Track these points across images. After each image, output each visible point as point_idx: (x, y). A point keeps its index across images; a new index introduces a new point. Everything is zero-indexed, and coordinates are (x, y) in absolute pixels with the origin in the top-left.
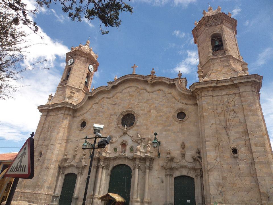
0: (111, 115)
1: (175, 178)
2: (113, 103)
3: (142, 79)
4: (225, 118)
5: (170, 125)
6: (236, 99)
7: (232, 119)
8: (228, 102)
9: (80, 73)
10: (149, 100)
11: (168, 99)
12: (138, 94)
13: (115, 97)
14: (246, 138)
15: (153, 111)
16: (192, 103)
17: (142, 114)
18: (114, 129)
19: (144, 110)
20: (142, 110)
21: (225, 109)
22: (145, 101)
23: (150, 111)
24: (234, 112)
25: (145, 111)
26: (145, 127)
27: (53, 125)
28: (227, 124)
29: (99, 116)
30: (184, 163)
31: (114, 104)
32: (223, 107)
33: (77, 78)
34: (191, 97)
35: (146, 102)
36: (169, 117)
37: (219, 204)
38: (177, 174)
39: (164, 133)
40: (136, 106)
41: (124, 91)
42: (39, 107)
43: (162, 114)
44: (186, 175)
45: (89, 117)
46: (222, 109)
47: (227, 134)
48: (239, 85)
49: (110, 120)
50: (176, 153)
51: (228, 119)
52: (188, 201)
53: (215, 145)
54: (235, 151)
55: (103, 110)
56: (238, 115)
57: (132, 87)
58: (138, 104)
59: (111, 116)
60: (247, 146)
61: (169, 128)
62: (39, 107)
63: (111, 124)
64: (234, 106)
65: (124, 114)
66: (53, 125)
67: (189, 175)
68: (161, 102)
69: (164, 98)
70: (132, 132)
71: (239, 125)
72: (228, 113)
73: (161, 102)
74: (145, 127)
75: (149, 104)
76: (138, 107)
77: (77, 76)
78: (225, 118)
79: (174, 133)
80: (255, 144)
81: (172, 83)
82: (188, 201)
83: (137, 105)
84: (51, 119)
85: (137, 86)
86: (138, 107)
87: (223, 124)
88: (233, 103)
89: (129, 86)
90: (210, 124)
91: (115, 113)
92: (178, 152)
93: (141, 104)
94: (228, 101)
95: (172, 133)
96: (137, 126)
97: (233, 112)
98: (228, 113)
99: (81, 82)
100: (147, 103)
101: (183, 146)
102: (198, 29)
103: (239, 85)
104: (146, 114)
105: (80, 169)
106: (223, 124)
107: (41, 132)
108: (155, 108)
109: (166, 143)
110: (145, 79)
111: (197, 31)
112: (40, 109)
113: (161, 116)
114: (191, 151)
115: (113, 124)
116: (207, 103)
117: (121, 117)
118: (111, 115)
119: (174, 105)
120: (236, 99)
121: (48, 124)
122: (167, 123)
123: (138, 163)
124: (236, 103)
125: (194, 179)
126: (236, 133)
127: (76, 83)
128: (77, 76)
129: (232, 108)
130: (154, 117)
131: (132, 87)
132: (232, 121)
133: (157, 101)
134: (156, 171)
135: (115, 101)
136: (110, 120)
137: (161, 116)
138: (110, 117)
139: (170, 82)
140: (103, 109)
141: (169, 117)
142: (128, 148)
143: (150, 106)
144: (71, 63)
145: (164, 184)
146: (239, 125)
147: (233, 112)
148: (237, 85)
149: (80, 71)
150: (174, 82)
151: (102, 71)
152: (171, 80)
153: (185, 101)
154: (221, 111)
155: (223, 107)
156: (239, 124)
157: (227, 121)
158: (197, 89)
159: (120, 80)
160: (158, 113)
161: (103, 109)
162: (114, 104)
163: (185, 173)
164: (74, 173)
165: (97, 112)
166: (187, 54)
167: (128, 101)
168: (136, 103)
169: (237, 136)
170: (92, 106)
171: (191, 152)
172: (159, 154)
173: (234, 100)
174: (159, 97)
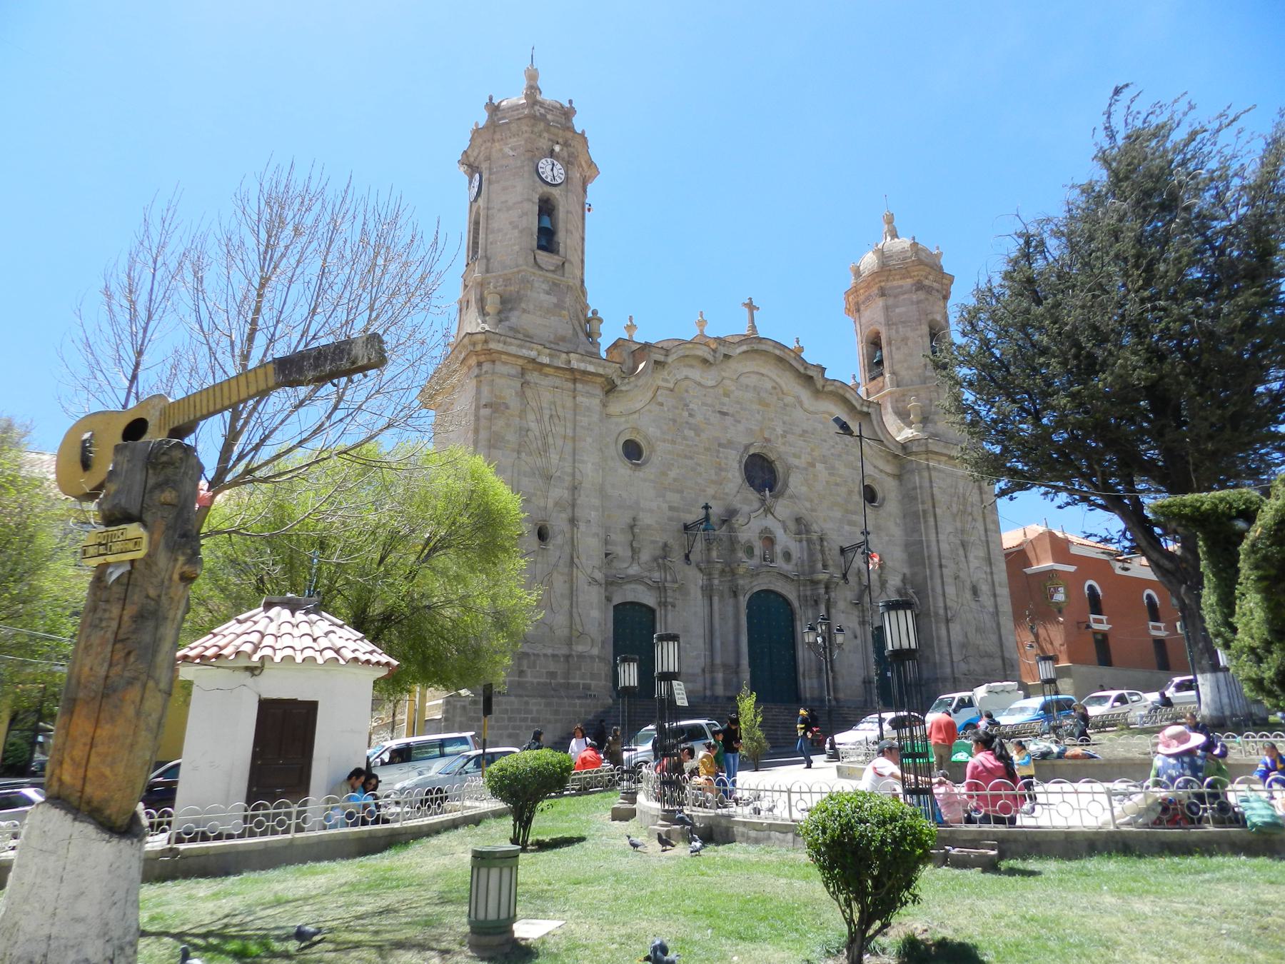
2: (718, 408)
3: (802, 370)
15: (819, 466)
16: (890, 472)
20: (795, 456)
29: (685, 438)
30: (634, 570)
34: (890, 458)
35: (801, 436)
37: (268, 960)
38: (617, 600)
39: (847, 528)
43: (838, 480)
58: (784, 436)
68: (833, 447)
73: (833, 447)
74: (808, 505)
81: (865, 409)
85: (778, 380)
86: (784, 444)
89: (756, 369)
93: (790, 438)
104: (806, 469)
105: (596, 571)
108: (824, 460)
110: (810, 373)
123: (163, 495)
131: (763, 375)
135: (724, 404)
142: (778, 549)
143: (812, 450)
145: (859, 641)
151: (1061, 619)
161: (691, 415)
168: (779, 431)
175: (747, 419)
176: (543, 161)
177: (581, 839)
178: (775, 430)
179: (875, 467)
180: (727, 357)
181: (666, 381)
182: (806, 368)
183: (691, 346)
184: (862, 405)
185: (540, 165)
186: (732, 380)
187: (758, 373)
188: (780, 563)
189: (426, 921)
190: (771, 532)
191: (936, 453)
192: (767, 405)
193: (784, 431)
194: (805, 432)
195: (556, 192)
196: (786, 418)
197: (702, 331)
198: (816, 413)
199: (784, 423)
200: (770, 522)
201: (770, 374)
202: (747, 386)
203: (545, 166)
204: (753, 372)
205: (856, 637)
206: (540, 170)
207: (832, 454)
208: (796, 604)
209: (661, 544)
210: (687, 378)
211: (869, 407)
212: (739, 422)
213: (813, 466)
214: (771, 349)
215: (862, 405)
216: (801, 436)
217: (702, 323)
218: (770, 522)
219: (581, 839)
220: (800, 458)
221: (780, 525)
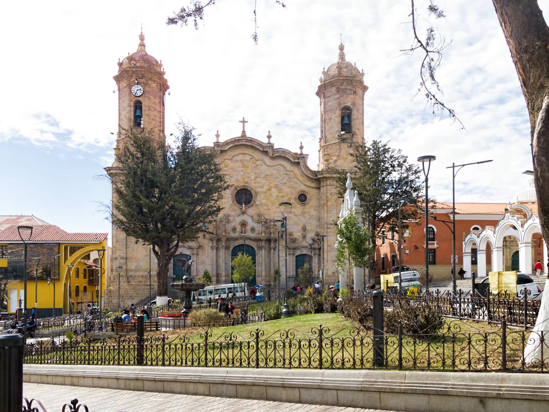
1: (297, 257)
3: (261, 149)
11: (290, 178)
12: (255, 165)
15: (273, 190)
17: (262, 192)
20: (260, 187)
22: (263, 176)
26: (266, 207)
35: (264, 178)
36: (291, 198)
38: (298, 253)
41: (235, 158)
50: (297, 235)
57: (245, 154)
69: (285, 176)
74: (266, 207)
77: (153, 119)
81: (297, 161)
85: (253, 154)
86: (255, 183)
89: (241, 152)
92: (300, 234)
93: (258, 180)
96: (257, 205)
101: (304, 229)
104: (266, 192)
119: (296, 185)
130: (275, 197)
131: (245, 154)
139: (294, 159)
141: (291, 198)
142: (248, 228)
143: (270, 183)
144: (136, 95)
150: (299, 161)
153: (309, 183)
163: (305, 252)
168: (253, 177)
175: (236, 175)
176: (134, 87)
178: (250, 177)
180: (222, 152)
182: (263, 148)
185: (133, 89)
188: (250, 234)
190: (245, 221)
192: (248, 167)
193: (255, 177)
194: (266, 175)
195: (140, 99)
196: (256, 171)
199: (256, 173)
200: (245, 217)
202: (237, 160)
203: (135, 89)
207: (281, 183)
208: (256, 249)
211: (298, 159)
212: (232, 177)
213: (270, 190)
216: (264, 178)
218: (245, 217)
220: (263, 187)
221: (250, 218)
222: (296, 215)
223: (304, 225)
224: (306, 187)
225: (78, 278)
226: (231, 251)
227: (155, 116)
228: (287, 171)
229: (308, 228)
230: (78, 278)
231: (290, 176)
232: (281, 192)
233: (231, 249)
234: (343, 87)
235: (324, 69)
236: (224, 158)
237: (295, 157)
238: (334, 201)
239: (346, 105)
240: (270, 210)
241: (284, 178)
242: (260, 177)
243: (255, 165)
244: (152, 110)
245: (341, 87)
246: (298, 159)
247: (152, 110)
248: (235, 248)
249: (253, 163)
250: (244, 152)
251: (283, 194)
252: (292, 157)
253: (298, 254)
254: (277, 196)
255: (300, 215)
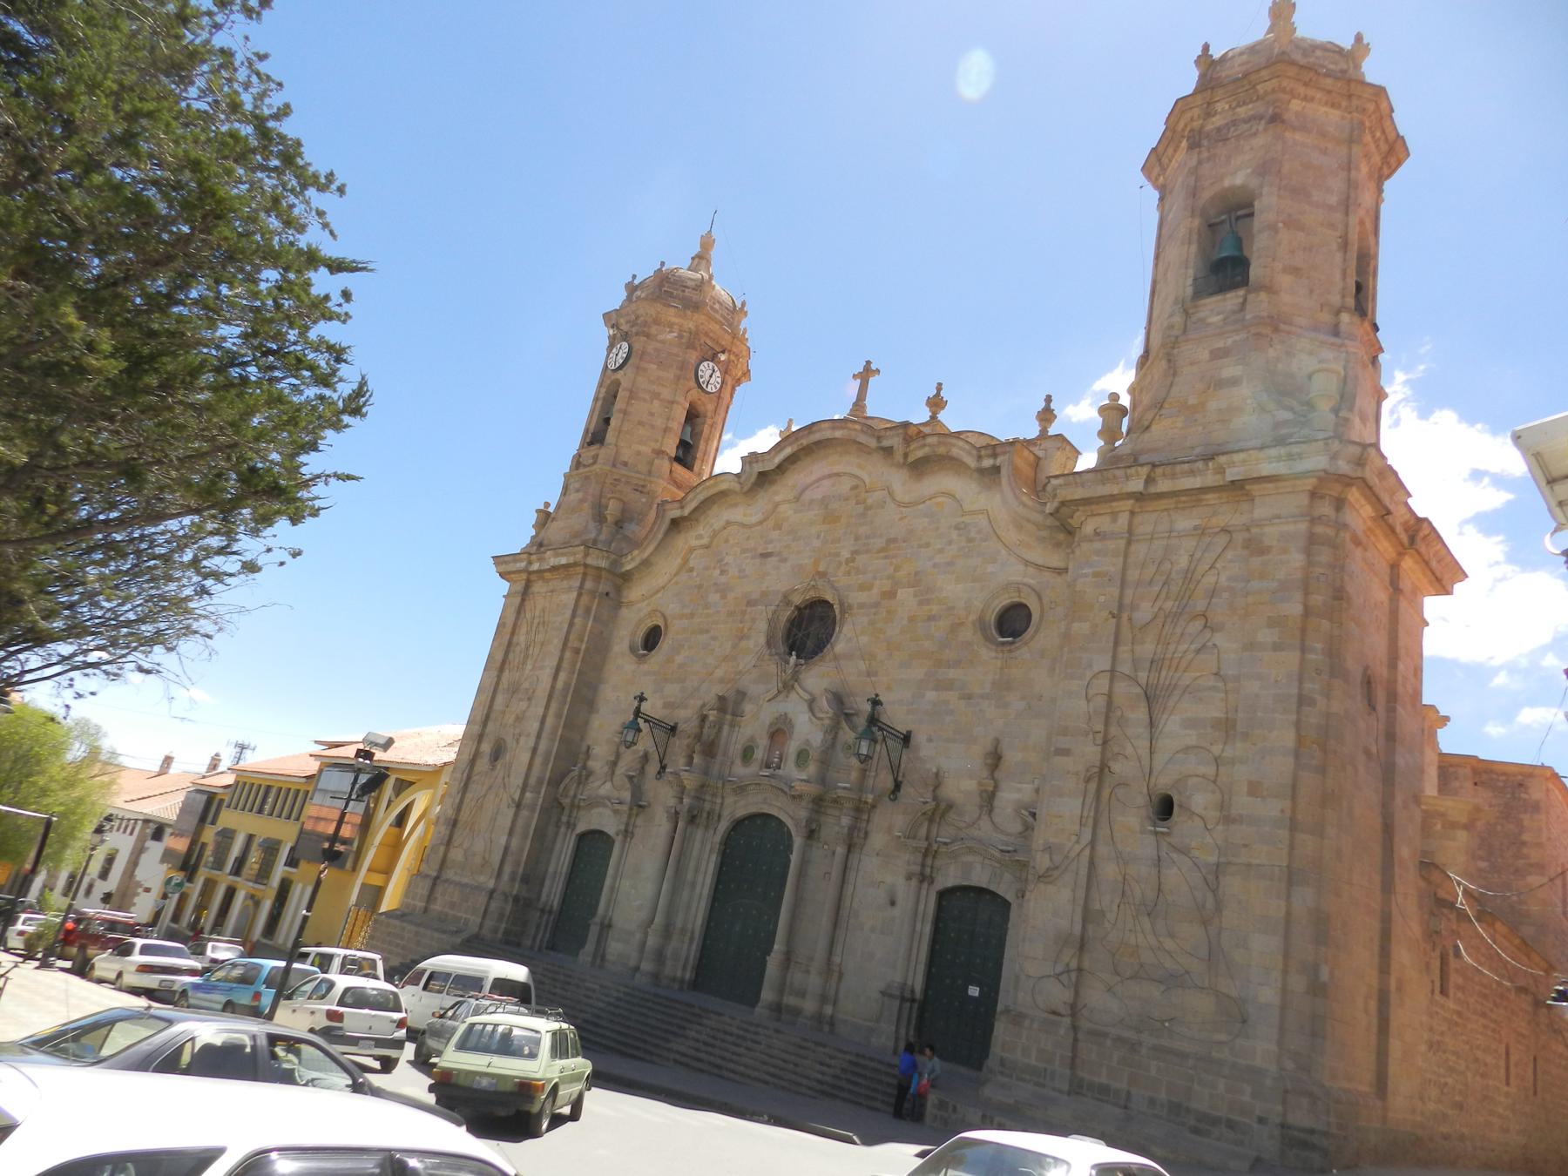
0: (750, 603)
1: (943, 895)
4: (1159, 651)
5: (957, 664)
6: (1231, 561)
7: (1190, 656)
8: (1189, 575)
9: (656, 402)
10: (894, 540)
11: (970, 540)
12: (861, 508)
13: (771, 523)
14: (1224, 754)
15: (904, 594)
17: (861, 606)
18: (753, 663)
19: (870, 588)
20: (862, 588)
21: (1169, 605)
22: (879, 543)
23: (890, 595)
24: (1205, 626)
25: (875, 591)
26: (863, 666)
27: (540, 637)
28: (1161, 681)
29: (707, 606)
31: (765, 556)
32: (1163, 595)
33: (642, 431)
35: (880, 551)
36: (962, 624)
38: (950, 877)
39: (931, 695)
40: (843, 568)
42: (498, 560)
44: (984, 886)
45: (672, 606)
46: (1158, 604)
47: (1152, 724)
48: (1255, 488)
49: (741, 626)
50: (962, 786)
51: (1169, 656)
52: (974, 991)
53: (1087, 771)
54: (1165, 808)
55: (723, 579)
56: (1219, 639)
59: (749, 609)
60: (1220, 789)
61: (952, 673)
62: (498, 560)
63: (743, 644)
64: (1213, 593)
65: (797, 600)
66: (540, 637)
67: (992, 888)
68: (941, 551)
69: (954, 535)
70: (818, 678)
71: (1214, 688)
72: (1178, 630)
73: (941, 551)
74: (863, 666)
75: (894, 561)
76: (849, 573)
77: (641, 423)
78: (1159, 651)
79: (969, 697)
80: (1250, 783)
81: (987, 463)
82: (974, 991)
83: (847, 561)
84: (537, 614)
86: (849, 573)
87: (1142, 676)
88: (1210, 580)
89: (826, 471)
90: (1089, 674)
91: (764, 594)
92: (970, 785)
93: (861, 560)
94: (1192, 567)
95: (960, 698)
96: (836, 658)
97: (1198, 624)
98: (1178, 630)
99: (657, 446)
100: (886, 557)
101: (995, 759)
102: (1165, 160)
103: (1255, 488)
104: (877, 605)
106: (1143, 681)
107: (504, 662)
109: (930, 740)
111: (1165, 170)
112: (503, 568)
113: (931, 618)
114: (1019, 786)
115: (751, 644)
116: (1096, 575)
117: (786, 614)
118: (750, 603)
119: (990, 568)
120: (1231, 561)
121: (527, 633)
122: (947, 651)
124: (1223, 578)
125: (1009, 904)
126: (1191, 723)
127: (639, 453)
128: (641, 423)
129: (1200, 605)
130: (905, 622)
131: (838, 475)
132: (1184, 664)
133: (928, 545)
134: (878, 854)
135: (771, 541)
136: (741, 626)
137: (931, 618)
138: (744, 613)
140: (722, 572)
141: (962, 624)
143: (897, 569)
146: (1214, 688)
147: (1198, 624)
148: (1242, 488)
149: (656, 396)
150: (998, 461)
152: (983, 453)
154: (1149, 616)
155: (1163, 595)
156: (1212, 682)
157: (1167, 663)
158: (1063, 503)
159: (790, 444)
160: (921, 603)
161: (722, 572)
162: (765, 556)
163: (979, 878)
164: (606, 830)
165: (700, 587)
166: (342, 421)
167: (817, 543)
168: (846, 554)
169: (1191, 738)
170: (686, 561)
171: (1019, 790)
172: (898, 786)
173: (1218, 565)
174: (937, 529)
177: (316, 742)
178: (838, 555)
179: (1027, 563)
181: (700, 537)
182: (879, 439)
183: (712, 482)
184: (980, 458)
186: (789, 501)
187: (830, 476)
189: (174, 337)
191: (1086, 502)
197: (934, 417)
198: (916, 503)
199: (857, 539)
201: (848, 469)
202: (812, 501)
204: (824, 478)
205: (893, 903)
206: (700, 373)
207: (935, 566)
209: (641, 753)
210: (728, 523)
211: (995, 456)
214: (828, 434)
215: (980, 458)
217: (936, 403)
219: (316, 742)
222: (969, 697)
223: (997, 742)
224: (1031, 570)
225: (287, 106)
226: (718, 838)
227: (652, 414)
228: (964, 513)
229: (1012, 757)
230: (287, 106)
231: (973, 534)
232: (928, 602)
233: (724, 826)
234: (1218, 121)
235: (634, 277)
236: (777, 498)
237: (979, 449)
238: (1105, 614)
239: (1227, 183)
240: (876, 674)
241: (950, 543)
242: (867, 552)
243: (861, 508)
244: (645, 400)
245: (1209, 127)
246: (995, 456)
247: (645, 400)
248: (738, 825)
249: (857, 503)
250: (836, 469)
251: (935, 609)
252: (969, 453)
253: (950, 883)
254: (912, 619)
255: (983, 697)
